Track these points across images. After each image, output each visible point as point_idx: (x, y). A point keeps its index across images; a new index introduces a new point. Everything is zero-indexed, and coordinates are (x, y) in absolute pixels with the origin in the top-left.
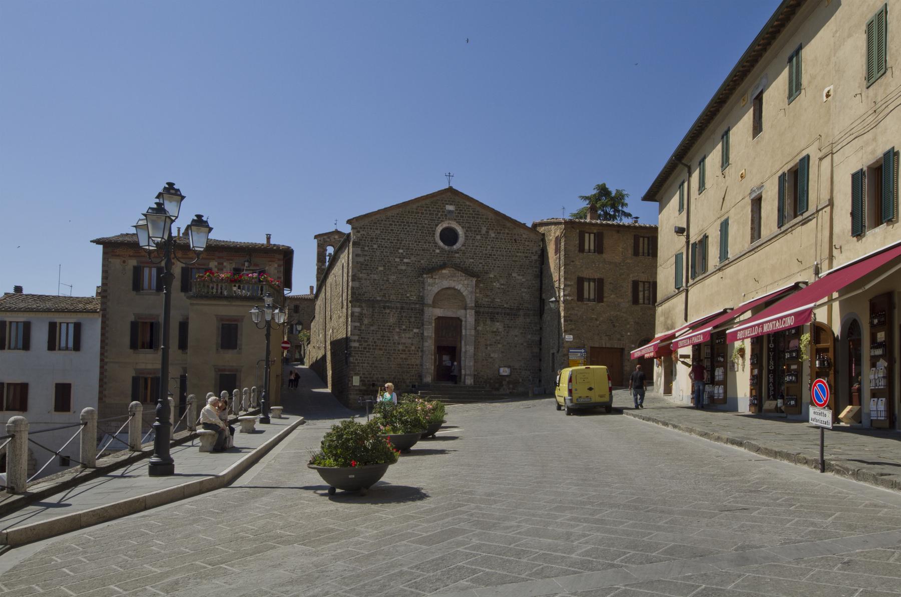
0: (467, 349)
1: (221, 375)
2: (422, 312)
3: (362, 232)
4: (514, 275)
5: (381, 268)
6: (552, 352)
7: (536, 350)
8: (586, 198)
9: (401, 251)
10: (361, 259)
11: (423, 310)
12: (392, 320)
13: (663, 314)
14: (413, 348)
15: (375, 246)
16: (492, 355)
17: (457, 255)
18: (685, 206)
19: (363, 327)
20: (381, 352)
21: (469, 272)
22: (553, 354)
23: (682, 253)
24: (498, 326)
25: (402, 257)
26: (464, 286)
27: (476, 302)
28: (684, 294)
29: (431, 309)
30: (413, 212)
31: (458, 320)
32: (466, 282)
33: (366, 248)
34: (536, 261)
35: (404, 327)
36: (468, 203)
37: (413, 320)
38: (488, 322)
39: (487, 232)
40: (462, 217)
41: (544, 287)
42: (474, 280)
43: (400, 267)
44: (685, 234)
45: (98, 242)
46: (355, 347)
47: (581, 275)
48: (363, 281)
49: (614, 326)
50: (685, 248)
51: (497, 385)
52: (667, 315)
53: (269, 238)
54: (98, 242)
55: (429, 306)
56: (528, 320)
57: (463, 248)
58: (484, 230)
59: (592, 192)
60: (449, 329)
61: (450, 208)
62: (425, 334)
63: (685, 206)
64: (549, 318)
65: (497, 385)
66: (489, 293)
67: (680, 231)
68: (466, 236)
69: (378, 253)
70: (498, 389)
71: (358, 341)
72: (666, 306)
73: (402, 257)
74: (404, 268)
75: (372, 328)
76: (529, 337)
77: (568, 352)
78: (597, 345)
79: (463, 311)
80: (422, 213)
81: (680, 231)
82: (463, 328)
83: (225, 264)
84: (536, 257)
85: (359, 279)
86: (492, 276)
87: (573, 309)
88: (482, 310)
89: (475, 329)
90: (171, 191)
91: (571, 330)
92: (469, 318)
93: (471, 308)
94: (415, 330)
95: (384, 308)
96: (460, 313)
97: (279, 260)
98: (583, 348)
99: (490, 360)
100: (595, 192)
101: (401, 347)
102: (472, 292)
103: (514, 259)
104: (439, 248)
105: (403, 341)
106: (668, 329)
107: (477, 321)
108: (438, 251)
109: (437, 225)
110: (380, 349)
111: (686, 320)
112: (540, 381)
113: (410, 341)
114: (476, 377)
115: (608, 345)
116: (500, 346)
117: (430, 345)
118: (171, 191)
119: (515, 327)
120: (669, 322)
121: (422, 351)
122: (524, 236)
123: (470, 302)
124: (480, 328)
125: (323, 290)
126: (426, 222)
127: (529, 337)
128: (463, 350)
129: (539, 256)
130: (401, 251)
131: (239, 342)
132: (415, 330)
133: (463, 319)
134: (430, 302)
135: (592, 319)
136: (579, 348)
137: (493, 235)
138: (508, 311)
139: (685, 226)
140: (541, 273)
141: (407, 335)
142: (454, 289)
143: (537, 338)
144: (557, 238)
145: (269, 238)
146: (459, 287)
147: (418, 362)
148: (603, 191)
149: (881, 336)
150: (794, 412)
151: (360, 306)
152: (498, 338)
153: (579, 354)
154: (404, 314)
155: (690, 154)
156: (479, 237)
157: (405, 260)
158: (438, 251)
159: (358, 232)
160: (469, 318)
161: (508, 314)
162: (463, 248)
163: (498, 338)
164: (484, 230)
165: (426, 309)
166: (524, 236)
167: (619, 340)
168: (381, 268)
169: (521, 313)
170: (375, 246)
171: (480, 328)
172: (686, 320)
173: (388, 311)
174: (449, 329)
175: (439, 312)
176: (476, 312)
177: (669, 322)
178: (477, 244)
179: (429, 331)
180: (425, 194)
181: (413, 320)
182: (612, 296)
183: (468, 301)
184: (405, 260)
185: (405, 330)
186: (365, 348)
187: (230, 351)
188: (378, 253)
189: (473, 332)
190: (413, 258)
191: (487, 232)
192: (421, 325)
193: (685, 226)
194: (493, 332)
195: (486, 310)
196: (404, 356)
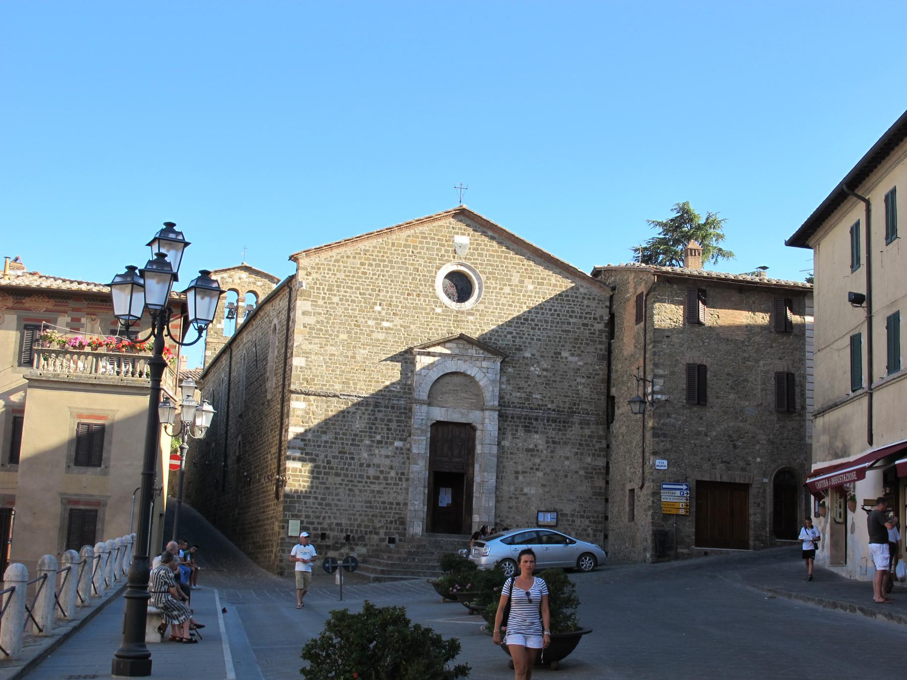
0: (483, 478)
1: (71, 510)
2: (407, 412)
3: (314, 275)
4: (565, 354)
5: (343, 336)
6: (629, 487)
7: (600, 483)
8: (660, 224)
11: (410, 410)
13: (825, 430)
14: (393, 474)
16: (526, 490)
17: (471, 318)
18: (863, 260)
20: (338, 480)
22: (632, 491)
23: (860, 334)
24: (537, 439)
25: (379, 319)
27: (501, 398)
28: (865, 400)
29: (425, 408)
30: (399, 245)
31: (470, 428)
32: (485, 364)
33: (321, 302)
34: (601, 331)
35: (378, 437)
38: (521, 433)
39: (522, 282)
40: (480, 255)
41: (614, 376)
42: (499, 360)
43: (375, 336)
44: (864, 304)
45: (393, 359)
49: (735, 447)
50: (866, 325)
52: (834, 432)
54: (393, 359)
55: (421, 402)
56: (587, 432)
57: (481, 307)
58: (516, 279)
59: (668, 215)
62: (415, 450)
63: (863, 260)
64: (623, 429)
66: (522, 384)
67: (856, 299)
69: (340, 311)
72: (831, 417)
74: (381, 336)
75: (325, 438)
76: (589, 460)
77: (660, 488)
78: (706, 478)
79: (478, 413)
80: (415, 247)
81: (856, 299)
82: (477, 442)
83: (83, 320)
84: (600, 326)
86: (528, 355)
87: (669, 416)
88: (510, 411)
89: (499, 444)
90: (169, 236)
91: (665, 451)
92: (487, 425)
93: (492, 409)
94: (398, 444)
96: (474, 417)
98: (685, 480)
99: (522, 498)
100: (674, 215)
101: (372, 472)
102: (493, 381)
103: (565, 327)
104: (442, 305)
105: (376, 461)
106: (837, 456)
107: (501, 431)
108: (439, 310)
109: (439, 268)
110: (337, 475)
111: (871, 442)
112: (606, 537)
113: (388, 462)
115: (725, 479)
117: (420, 469)
118: (169, 236)
119: (565, 443)
120: (839, 444)
121: (407, 480)
123: (490, 396)
124: (506, 443)
125: (207, 365)
126: (421, 261)
127: (589, 460)
128: (477, 479)
129: (606, 325)
131: (104, 455)
132: (398, 444)
133: (479, 427)
134: (424, 396)
135: (699, 433)
136: (677, 482)
137: (531, 287)
138: (553, 415)
139: (864, 292)
140: (609, 350)
141: (384, 452)
142: (464, 374)
143: (601, 462)
144: (639, 297)
146: (472, 371)
147: (400, 499)
148: (685, 215)
152: (537, 461)
153: (678, 493)
154: (380, 415)
155: (868, 183)
157: (385, 324)
160: (487, 425)
161: (554, 421)
163: (537, 461)
164: (516, 279)
165: (416, 407)
167: (743, 469)
168: (343, 336)
169: (576, 419)
170: (336, 299)
171: (506, 443)
172: (871, 442)
175: (439, 414)
176: (500, 416)
177: (839, 444)
178: (503, 300)
179: (420, 446)
180: (566, 262)
181: (393, 425)
182: (732, 396)
184: (385, 324)
185: (379, 442)
187: (91, 470)
188: (340, 311)
189: (495, 450)
192: (405, 434)
193: (864, 293)
194: (528, 450)
195: (518, 411)
196: (376, 487)
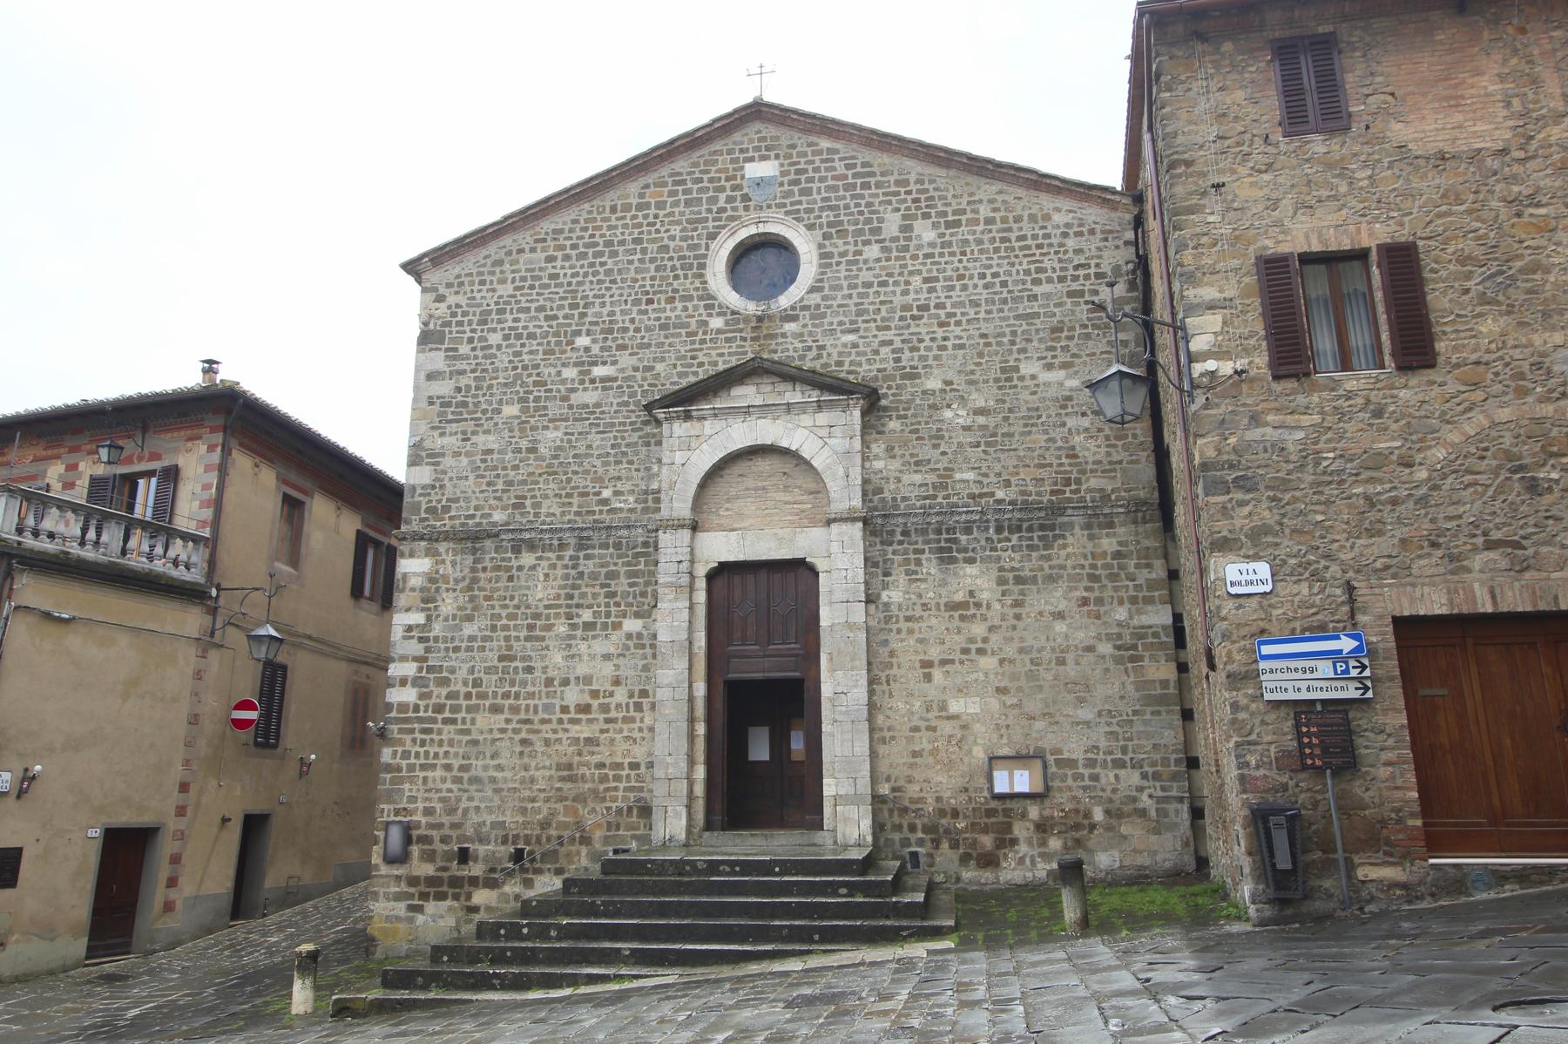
3: (452, 300)
4: (1027, 368)
5: (511, 410)
7: (1163, 671)
9: (583, 341)
10: (444, 388)
12: (541, 592)
14: (620, 695)
15: (495, 339)
16: (955, 706)
17: (790, 327)
19: (437, 629)
20: (498, 720)
21: (831, 386)
24: (975, 578)
25: (586, 363)
26: (822, 437)
27: (869, 489)
31: (800, 570)
35: (587, 616)
36: (825, 144)
37: (621, 585)
38: (930, 566)
39: (906, 229)
46: (403, 707)
47: (1274, 245)
48: (448, 462)
49: (1533, 487)
51: (987, 841)
53: (210, 366)
56: (1108, 544)
58: (892, 224)
60: (761, 608)
61: (764, 169)
65: (987, 841)
66: (926, 452)
68: (823, 256)
70: (989, 861)
71: (417, 682)
73: (586, 363)
74: (590, 397)
75: (469, 629)
76: (1121, 614)
78: (1435, 603)
85: (434, 457)
86: (934, 384)
87: (1256, 420)
89: (870, 600)
92: (839, 559)
95: (517, 550)
97: (213, 430)
99: (947, 728)
101: (573, 696)
105: (582, 669)
108: (717, 323)
110: (496, 709)
113: (608, 669)
114: (886, 807)
115: (1515, 600)
116: (988, 663)
119: (1051, 579)
122: (1058, 218)
123: (845, 494)
126: (676, 230)
127: (1121, 614)
130: (583, 341)
135: (1377, 462)
137: (929, 235)
141: (600, 647)
143: (1160, 617)
145: (210, 366)
149: (843, 891)
150: (1137, 690)
151: (430, 553)
152: (979, 629)
156: (873, 251)
157: (599, 371)
158: (717, 323)
159: (440, 299)
160: (839, 559)
162: (816, 298)
164: (892, 224)
166: (1058, 218)
173: (528, 559)
174: (761, 608)
175: (720, 547)
178: (866, 276)
179: (678, 620)
181: (621, 585)
183: (834, 486)
184: (599, 371)
185: (589, 626)
186: (439, 708)
188: (503, 359)
189: (859, 613)
190: (626, 360)
191: (906, 229)
194: (952, 606)
196: (583, 731)
